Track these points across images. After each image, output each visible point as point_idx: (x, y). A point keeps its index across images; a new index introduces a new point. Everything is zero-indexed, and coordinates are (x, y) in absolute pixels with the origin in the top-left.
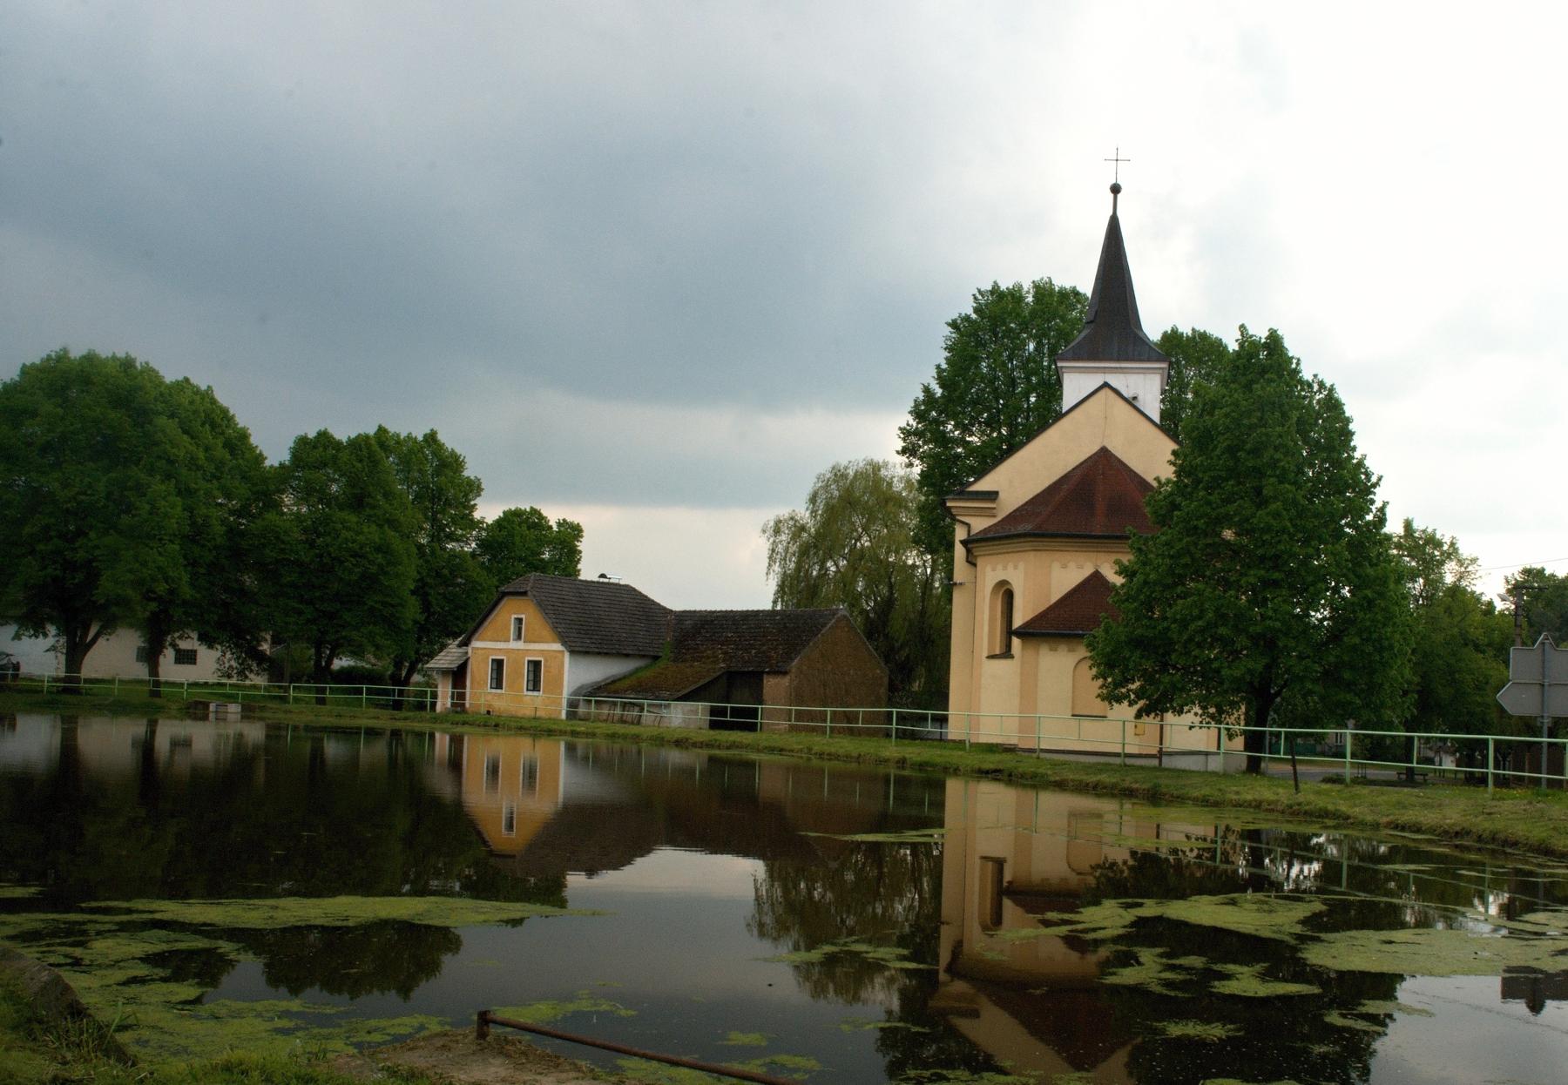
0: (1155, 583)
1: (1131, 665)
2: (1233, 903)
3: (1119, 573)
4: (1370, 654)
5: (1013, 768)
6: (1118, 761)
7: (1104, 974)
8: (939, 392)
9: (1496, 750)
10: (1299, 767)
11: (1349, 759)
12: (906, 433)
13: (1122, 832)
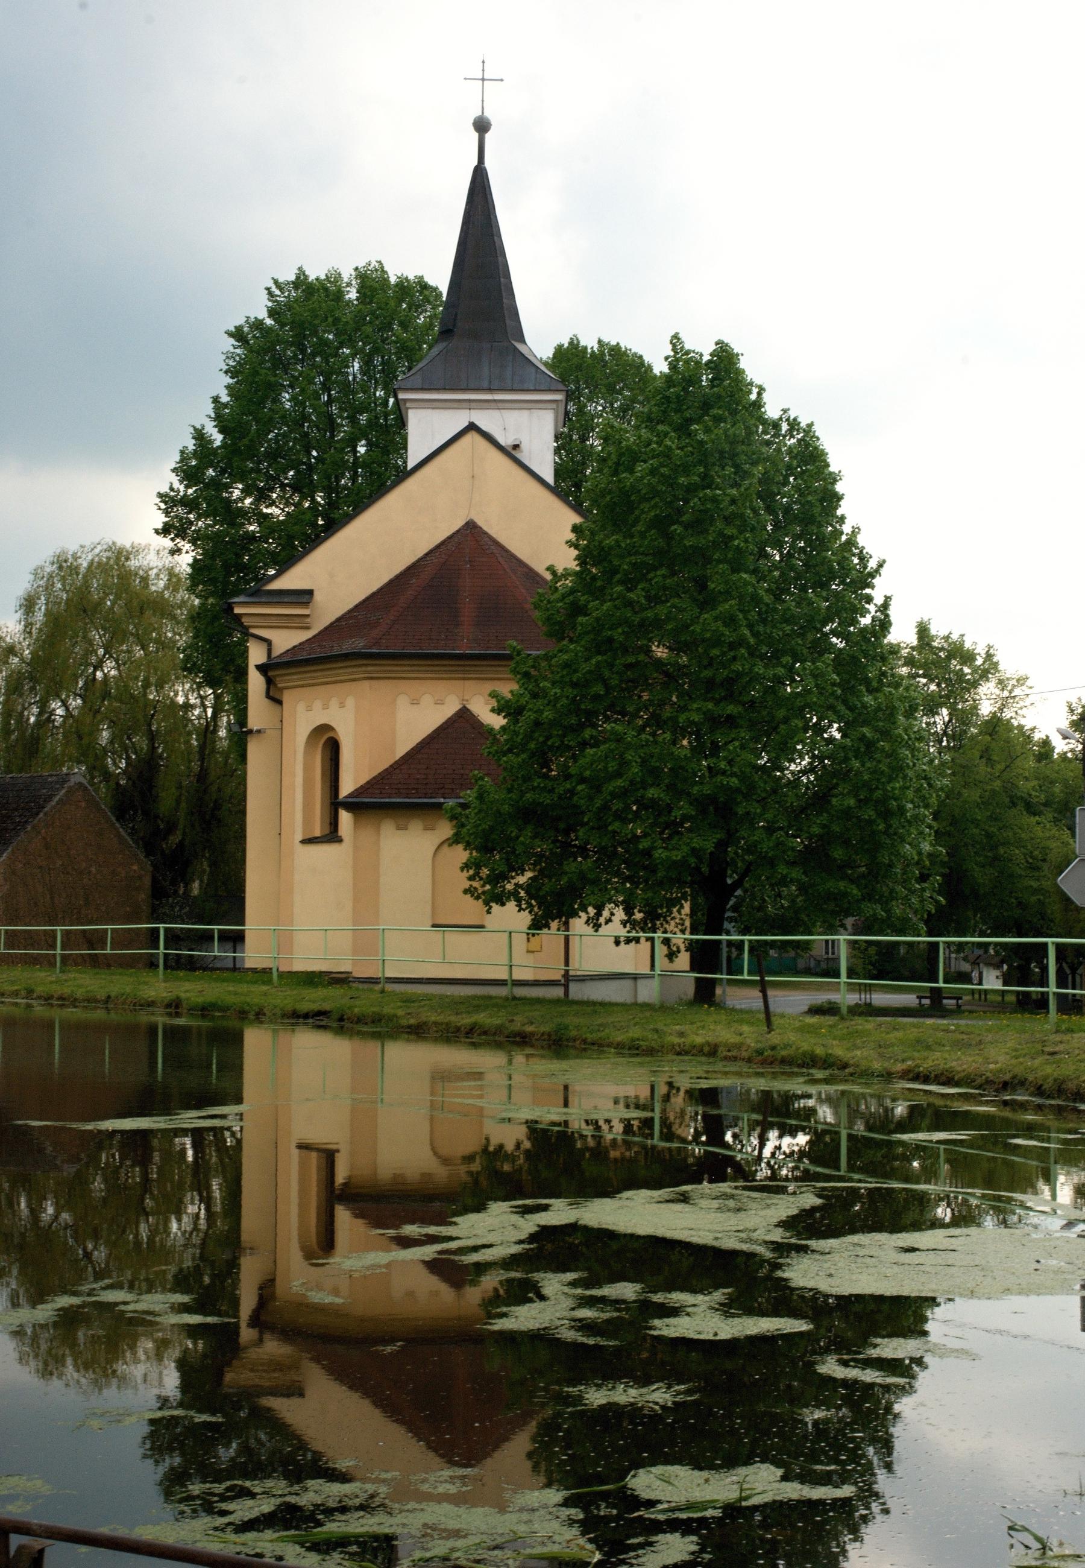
0: (553, 723)
1: (520, 849)
2: (684, 1199)
3: (497, 711)
4: (870, 822)
5: (348, 1007)
6: (503, 991)
7: (491, 1316)
8: (218, 439)
9: (1059, 959)
10: (770, 993)
11: (844, 978)
12: (169, 501)
13: (510, 1098)
